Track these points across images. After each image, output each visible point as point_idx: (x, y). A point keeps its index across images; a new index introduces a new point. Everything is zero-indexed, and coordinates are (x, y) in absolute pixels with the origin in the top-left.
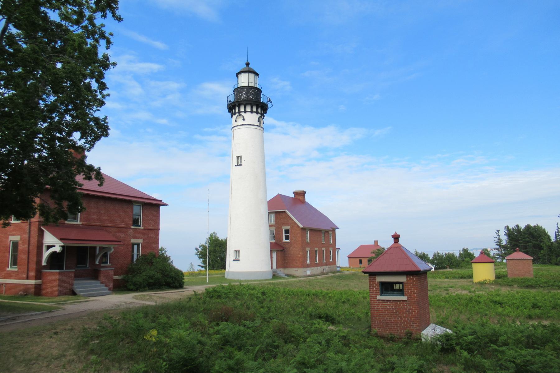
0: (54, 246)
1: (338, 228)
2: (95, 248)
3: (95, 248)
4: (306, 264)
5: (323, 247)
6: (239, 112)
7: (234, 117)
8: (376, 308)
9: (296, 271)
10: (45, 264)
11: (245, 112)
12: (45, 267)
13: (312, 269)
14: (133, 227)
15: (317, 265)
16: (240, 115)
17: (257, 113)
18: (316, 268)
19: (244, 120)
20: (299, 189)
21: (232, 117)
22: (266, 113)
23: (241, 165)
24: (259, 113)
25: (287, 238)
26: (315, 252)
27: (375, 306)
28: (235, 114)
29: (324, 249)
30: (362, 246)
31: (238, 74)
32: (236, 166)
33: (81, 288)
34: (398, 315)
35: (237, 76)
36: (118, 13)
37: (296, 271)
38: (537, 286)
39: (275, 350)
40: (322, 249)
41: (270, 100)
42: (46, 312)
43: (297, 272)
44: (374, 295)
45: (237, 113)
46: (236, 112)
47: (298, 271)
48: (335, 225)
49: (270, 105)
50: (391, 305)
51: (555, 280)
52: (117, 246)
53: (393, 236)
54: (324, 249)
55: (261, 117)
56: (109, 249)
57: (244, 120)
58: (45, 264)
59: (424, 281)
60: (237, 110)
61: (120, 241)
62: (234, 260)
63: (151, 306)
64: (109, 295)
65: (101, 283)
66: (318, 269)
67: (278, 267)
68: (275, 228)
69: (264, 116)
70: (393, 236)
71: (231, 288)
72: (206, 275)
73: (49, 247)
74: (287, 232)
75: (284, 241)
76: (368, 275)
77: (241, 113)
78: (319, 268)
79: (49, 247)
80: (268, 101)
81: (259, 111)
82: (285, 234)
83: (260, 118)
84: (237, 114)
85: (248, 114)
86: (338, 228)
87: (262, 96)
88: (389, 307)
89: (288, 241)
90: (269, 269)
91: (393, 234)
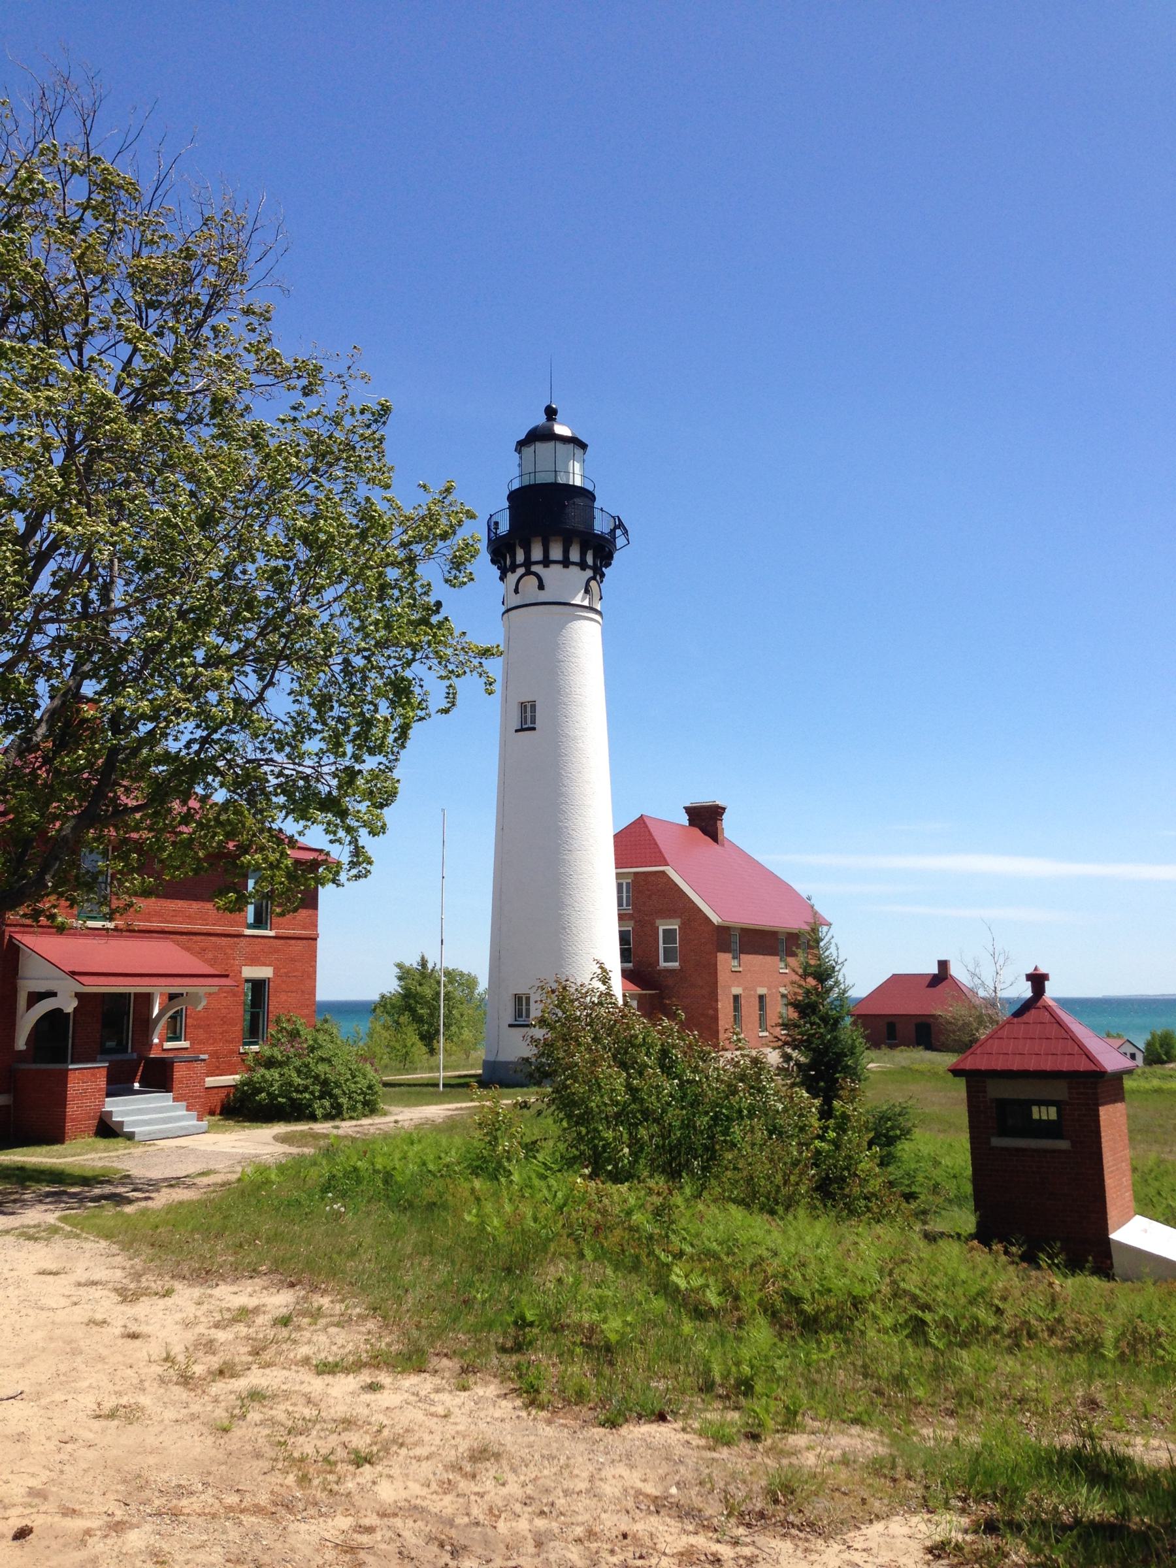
0: (54, 994)
2: (146, 999)
6: (528, 563)
7: (512, 578)
11: (546, 562)
16: (529, 572)
17: (583, 565)
19: (541, 587)
22: (608, 565)
23: (534, 729)
24: (589, 567)
28: (513, 569)
30: (896, 980)
32: (517, 731)
33: (140, 1112)
39: (725, 1258)
42: (426, 1093)
45: (520, 566)
46: (518, 562)
49: (620, 541)
52: (215, 989)
53: (1029, 977)
55: (594, 578)
56: (196, 998)
57: (541, 587)
60: (520, 557)
61: (227, 976)
62: (510, 1026)
63: (191, 1203)
65: (175, 1099)
68: (632, 923)
69: (603, 575)
70: (1029, 977)
71: (126, 1246)
73: (35, 998)
75: (663, 964)
79: (35, 998)
81: (590, 560)
84: (521, 571)
85: (556, 569)
87: (597, 513)
91: (1030, 970)
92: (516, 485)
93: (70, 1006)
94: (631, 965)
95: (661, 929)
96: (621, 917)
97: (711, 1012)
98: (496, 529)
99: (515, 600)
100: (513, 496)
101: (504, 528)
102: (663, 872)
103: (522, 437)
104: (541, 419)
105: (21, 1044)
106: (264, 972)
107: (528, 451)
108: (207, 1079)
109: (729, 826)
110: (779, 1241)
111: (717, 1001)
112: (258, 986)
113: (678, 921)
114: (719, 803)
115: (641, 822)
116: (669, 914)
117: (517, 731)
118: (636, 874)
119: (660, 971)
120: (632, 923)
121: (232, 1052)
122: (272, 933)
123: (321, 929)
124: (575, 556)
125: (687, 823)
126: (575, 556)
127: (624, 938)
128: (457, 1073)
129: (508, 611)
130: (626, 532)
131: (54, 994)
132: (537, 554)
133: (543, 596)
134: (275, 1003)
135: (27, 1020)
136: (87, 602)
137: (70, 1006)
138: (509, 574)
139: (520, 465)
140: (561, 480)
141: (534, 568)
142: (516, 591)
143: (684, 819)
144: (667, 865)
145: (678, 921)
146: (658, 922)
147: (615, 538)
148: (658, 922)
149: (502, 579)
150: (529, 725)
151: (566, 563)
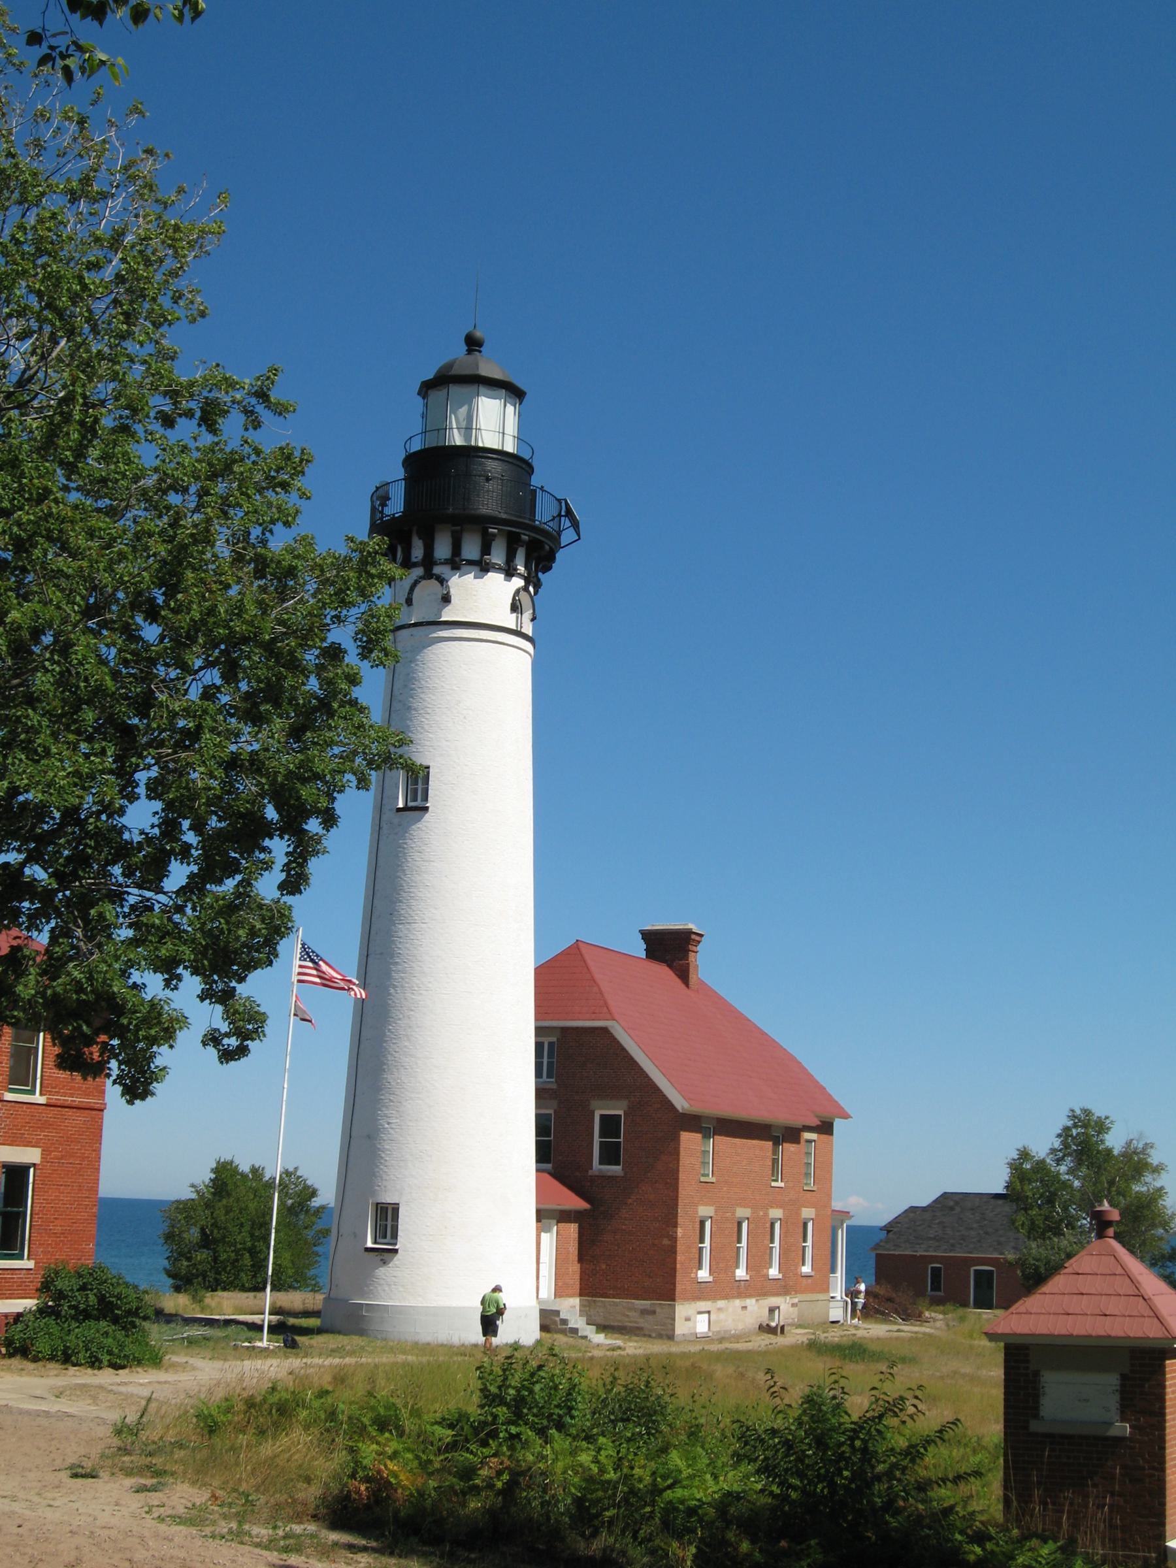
1: (846, 1116)
4: (715, 1281)
9: (644, 1312)
13: (720, 1309)
15: (741, 1290)
16: (429, 575)
18: (738, 1303)
25: (610, 1154)
26: (736, 1224)
29: (776, 1213)
30: (945, 1196)
31: (427, 388)
36: (424, 582)
37: (644, 1312)
38: (779, 1447)
40: (766, 1214)
41: (569, 513)
43: (650, 1318)
46: (414, 560)
48: (830, 1098)
49: (568, 536)
51: (44, 1484)
54: (776, 1213)
67: (559, 1293)
68: (555, 1103)
72: (263, 1313)
74: (610, 1125)
76: (543, 1234)
77: (437, 570)
78: (751, 1302)
80: (560, 515)
86: (846, 1116)
89: (616, 1169)
90: (533, 1303)
92: (416, 446)
106: (29, 1155)
111: (675, 1225)
116: (610, 1092)
120: (555, 1103)
125: (643, 955)
130: (575, 525)
132: (442, 550)
141: (437, 570)
143: (639, 948)
146: (594, 1103)
148: (594, 1103)
150: (418, 803)
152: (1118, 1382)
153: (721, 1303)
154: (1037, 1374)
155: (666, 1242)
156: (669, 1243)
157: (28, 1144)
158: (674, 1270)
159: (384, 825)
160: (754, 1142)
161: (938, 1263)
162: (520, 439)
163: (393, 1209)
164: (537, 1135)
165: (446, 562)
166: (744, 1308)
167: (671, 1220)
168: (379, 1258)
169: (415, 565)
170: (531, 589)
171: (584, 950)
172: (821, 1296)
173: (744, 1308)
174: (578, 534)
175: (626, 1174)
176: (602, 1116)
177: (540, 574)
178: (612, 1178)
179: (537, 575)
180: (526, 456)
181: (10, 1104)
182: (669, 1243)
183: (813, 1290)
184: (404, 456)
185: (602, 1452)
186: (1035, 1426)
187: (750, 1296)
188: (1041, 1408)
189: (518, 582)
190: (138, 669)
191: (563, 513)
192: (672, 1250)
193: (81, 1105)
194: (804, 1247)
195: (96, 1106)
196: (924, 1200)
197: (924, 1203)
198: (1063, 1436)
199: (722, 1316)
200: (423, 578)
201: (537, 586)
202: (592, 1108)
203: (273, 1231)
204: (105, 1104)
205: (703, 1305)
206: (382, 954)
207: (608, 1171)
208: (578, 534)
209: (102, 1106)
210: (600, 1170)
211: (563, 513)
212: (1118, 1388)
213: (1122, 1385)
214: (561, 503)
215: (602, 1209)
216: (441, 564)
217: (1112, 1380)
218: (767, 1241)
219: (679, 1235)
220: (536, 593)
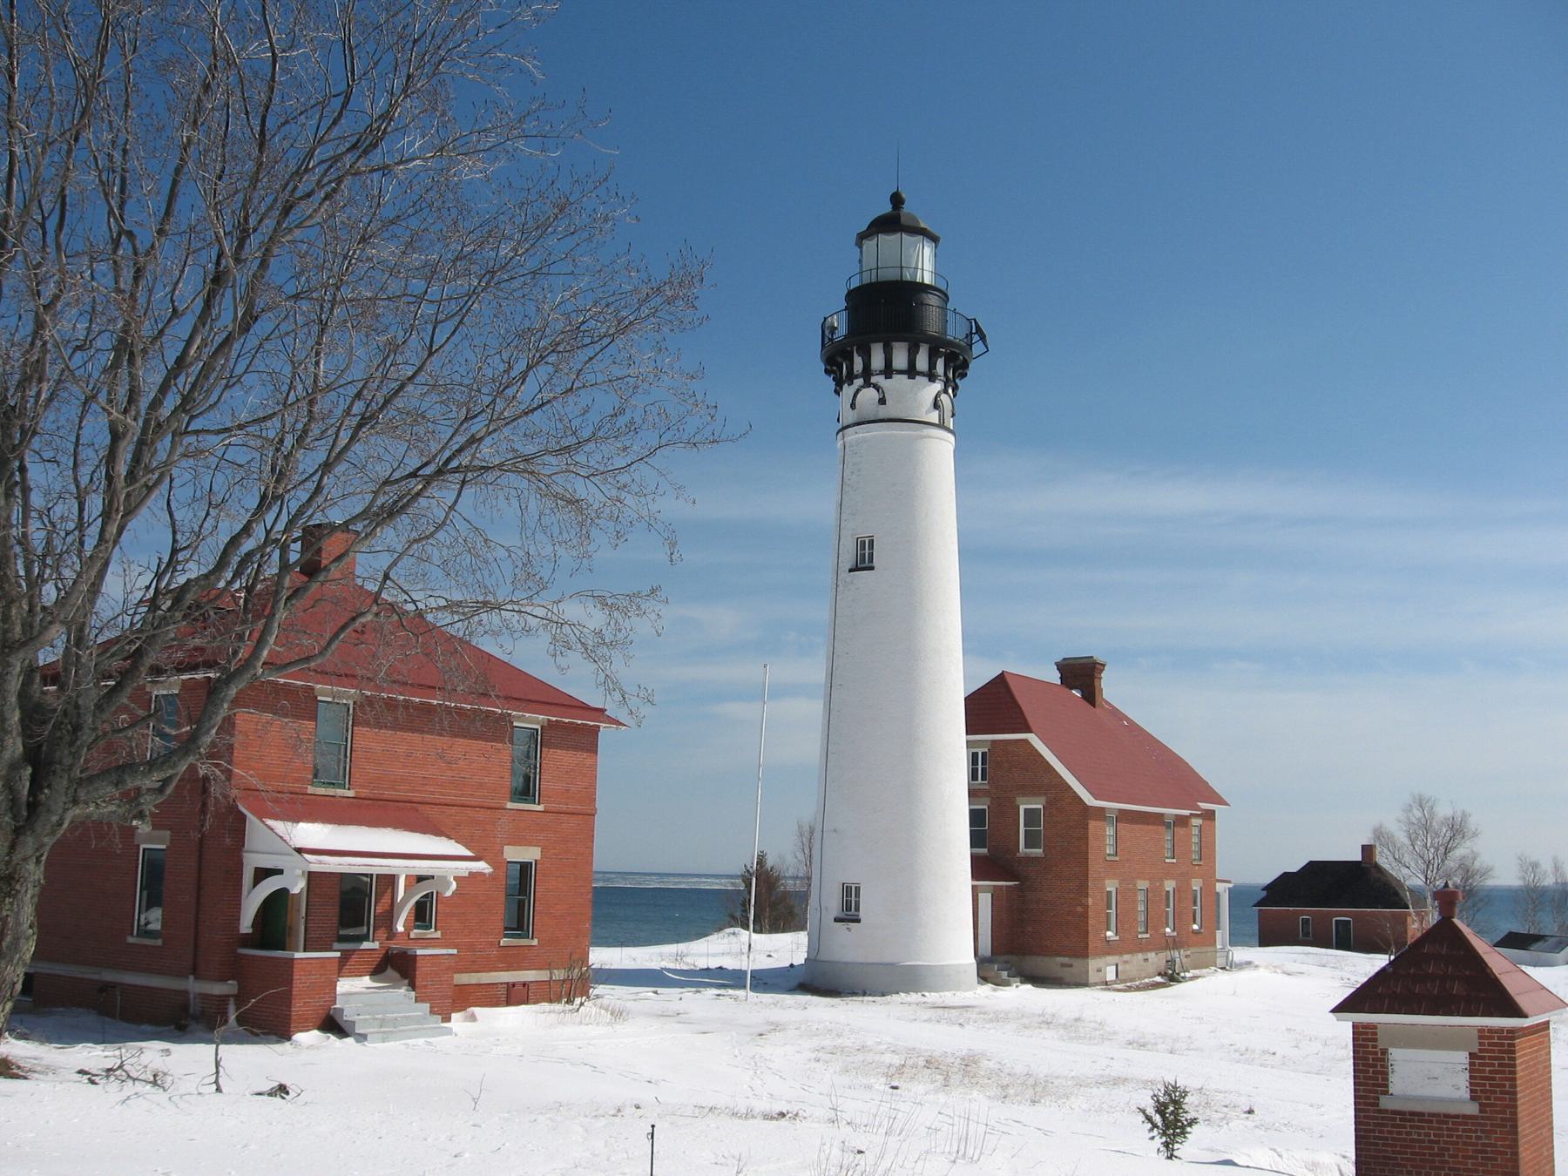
0: (280, 872)
3: (389, 881)
5: (1169, 876)
6: (867, 373)
7: (848, 391)
8: (1375, 1138)
10: (250, 931)
11: (888, 371)
12: (247, 941)
13: (1126, 962)
14: (510, 805)
16: (867, 384)
18: (1140, 956)
19: (882, 401)
20: (1077, 649)
21: (837, 392)
23: (872, 568)
25: (1031, 841)
27: (1371, 1131)
28: (851, 378)
34: (1448, 1162)
35: (859, 244)
37: (1063, 965)
41: (979, 330)
44: (1370, 1091)
46: (855, 372)
47: (1071, 966)
49: (978, 348)
50: (1423, 1128)
58: (250, 931)
59: (1537, 1051)
62: (836, 920)
64: (173, 988)
66: (1146, 960)
68: (987, 800)
73: (262, 874)
77: (874, 379)
78: (1151, 956)
79: (262, 874)
80: (971, 333)
82: (1025, 826)
83: (944, 397)
84: (859, 382)
85: (900, 381)
88: (1419, 1134)
89: (1038, 852)
92: (855, 283)
93: (298, 886)
94: (984, 851)
95: (1022, 808)
96: (973, 794)
97: (1079, 909)
98: (832, 333)
99: (849, 416)
100: (853, 296)
101: (842, 331)
102: (1026, 741)
103: (864, 228)
104: (887, 208)
105: (246, 924)
106: (530, 854)
107: (869, 245)
108: (456, 976)
109: (1111, 688)
110: (19, 856)
111: (1087, 896)
112: (525, 868)
113: (1043, 799)
114: (1099, 658)
115: (1001, 681)
116: (1031, 790)
117: (850, 571)
118: (994, 742)
119: (1020, 860)
120: (987, 800)
121: (492, 944)
122: (540, 808)
123: (599, 804)
124: (922, 362)
125: (1059, 683)
126: (922, 362)
127: (976, 817)
128: (140, 866)
129: (844, 428)
130: (983, 338)
131: (280, 872)
132: (878, 361)
133: (884, 412)
134: (541, 889)
135: (253, 901)
136: (520, 261)
137: (298, 886)
138: (845, 386)
139: (860, 261)
140: (908, 276)
141: (874, 379)
142: (853, 406)
143: (1054, 677)
144: (1030, 731)
145: (1043, 799)
146: (1019, 800)
147: (971, 346)
148: (1019, 800)
149: (837, 392)
150: (867, 564)
151: (911, 372)
152: (1467, 1061)
153: (1126, 957)
154: (1384, 1052)
155: (1079, 909)
156: (1083, 910)
157: (530, 844)
158: (1087, 932)
159: (839, 583)
160: (1150, 827)
161: (1306, 915)
162: (936, 274)
163: (856, 887)
164: (971, 826)
165: (881, 373)
166: (1146, 960)
167: (1083, 890)
168: (845, 927)
169: (857, 377)
170: (950, 391)
171: (1008, 679)
172: (1209, 949)
173: (1146, 960)
174: (987, 348)
175: (1046, 855)
176: (1025, 809)
177: (957, 381)
178: (1036, 859)
179: (954, 380)
180: (943, 288)
181: (512, 812)
182: (1083, 910)
183: (1204, 944)
184: (846, 292)
185: (953, 1159)
186: (1385, 1103)
187: (1151, 950)
188: (1391, 1084)
189: (938, 386)
190: (234, 329)
191: (974, 331)
192: (1085, 916)
193: (574, 811)
194: (1195, 910)
195: (589, 812)
196: (1295, 866)
197: (1295, 869)
198: (1413, 1113)
199: (1127, 967)
200: (863, 387)
201: (955, 389)
202: (1018, 803)
203: (752, 908)
204: (596, 810)
205: (1110, 959)
206: (841, 685)
207: (1031, 853)
208: (987, 348)
209: (594, 812)
210: (1026, 853)
211: (974, 331)
212: (1468, 1066)
213: (1471, 1064)
214: (971, 323)
215: (1028, 883)
216: (877, 374)
217: (1462, 1058)
218: (1163, 907)
219: (1090, 903)
220: (954, 396)
